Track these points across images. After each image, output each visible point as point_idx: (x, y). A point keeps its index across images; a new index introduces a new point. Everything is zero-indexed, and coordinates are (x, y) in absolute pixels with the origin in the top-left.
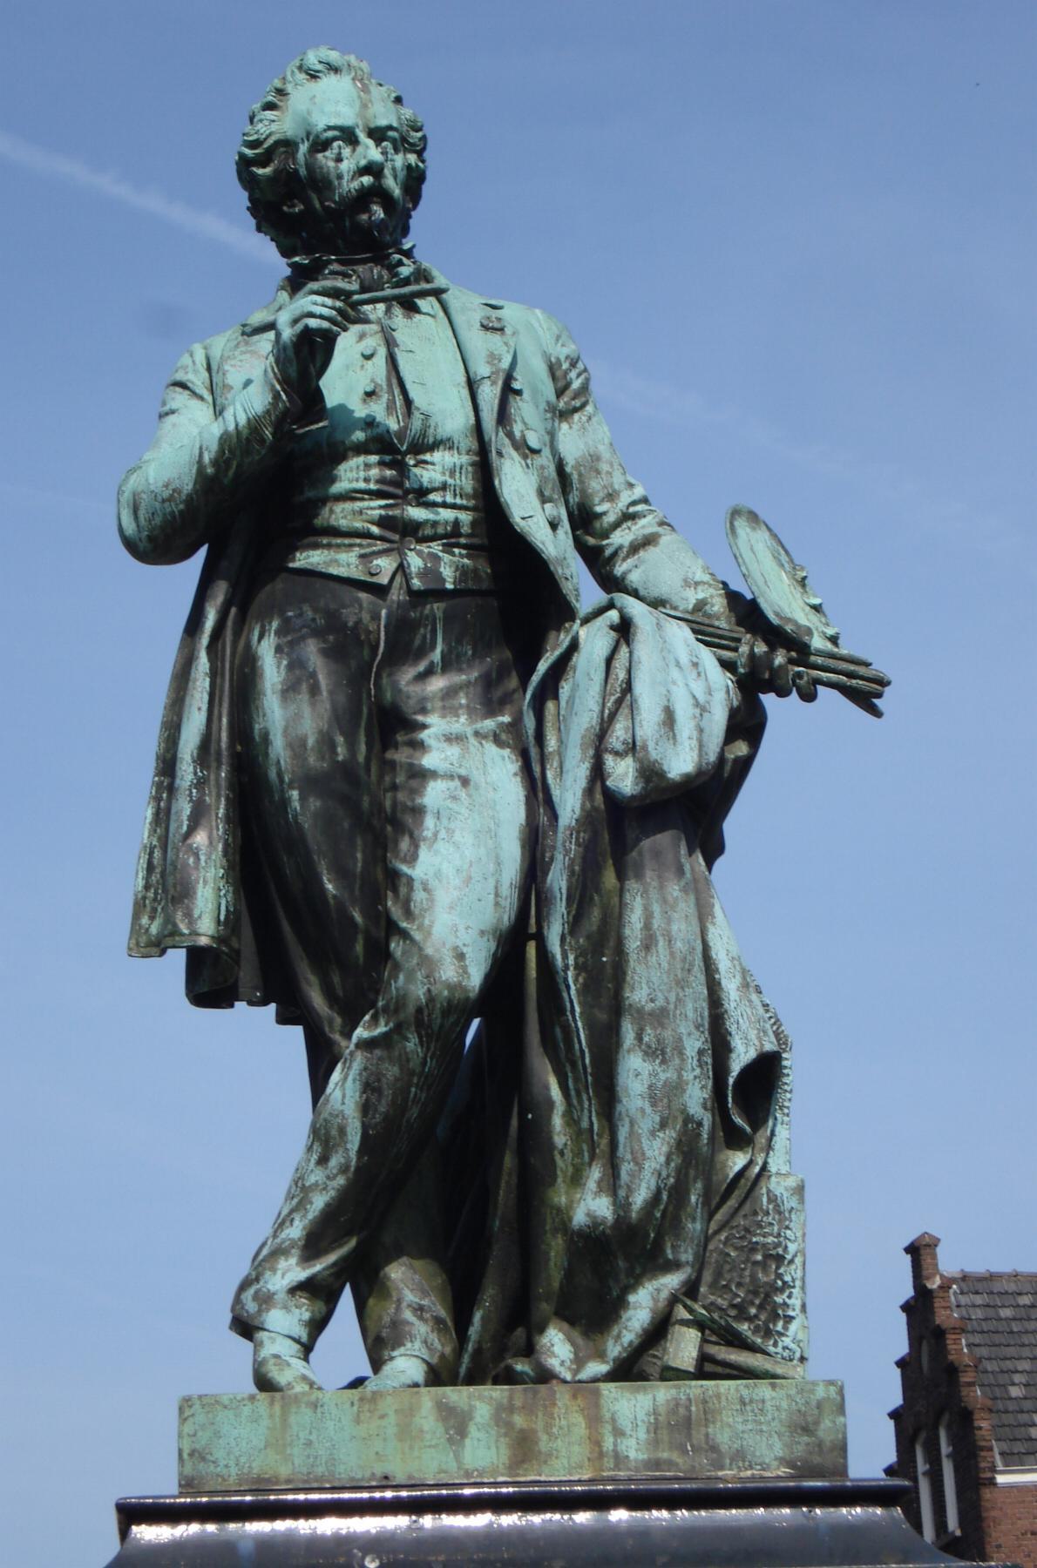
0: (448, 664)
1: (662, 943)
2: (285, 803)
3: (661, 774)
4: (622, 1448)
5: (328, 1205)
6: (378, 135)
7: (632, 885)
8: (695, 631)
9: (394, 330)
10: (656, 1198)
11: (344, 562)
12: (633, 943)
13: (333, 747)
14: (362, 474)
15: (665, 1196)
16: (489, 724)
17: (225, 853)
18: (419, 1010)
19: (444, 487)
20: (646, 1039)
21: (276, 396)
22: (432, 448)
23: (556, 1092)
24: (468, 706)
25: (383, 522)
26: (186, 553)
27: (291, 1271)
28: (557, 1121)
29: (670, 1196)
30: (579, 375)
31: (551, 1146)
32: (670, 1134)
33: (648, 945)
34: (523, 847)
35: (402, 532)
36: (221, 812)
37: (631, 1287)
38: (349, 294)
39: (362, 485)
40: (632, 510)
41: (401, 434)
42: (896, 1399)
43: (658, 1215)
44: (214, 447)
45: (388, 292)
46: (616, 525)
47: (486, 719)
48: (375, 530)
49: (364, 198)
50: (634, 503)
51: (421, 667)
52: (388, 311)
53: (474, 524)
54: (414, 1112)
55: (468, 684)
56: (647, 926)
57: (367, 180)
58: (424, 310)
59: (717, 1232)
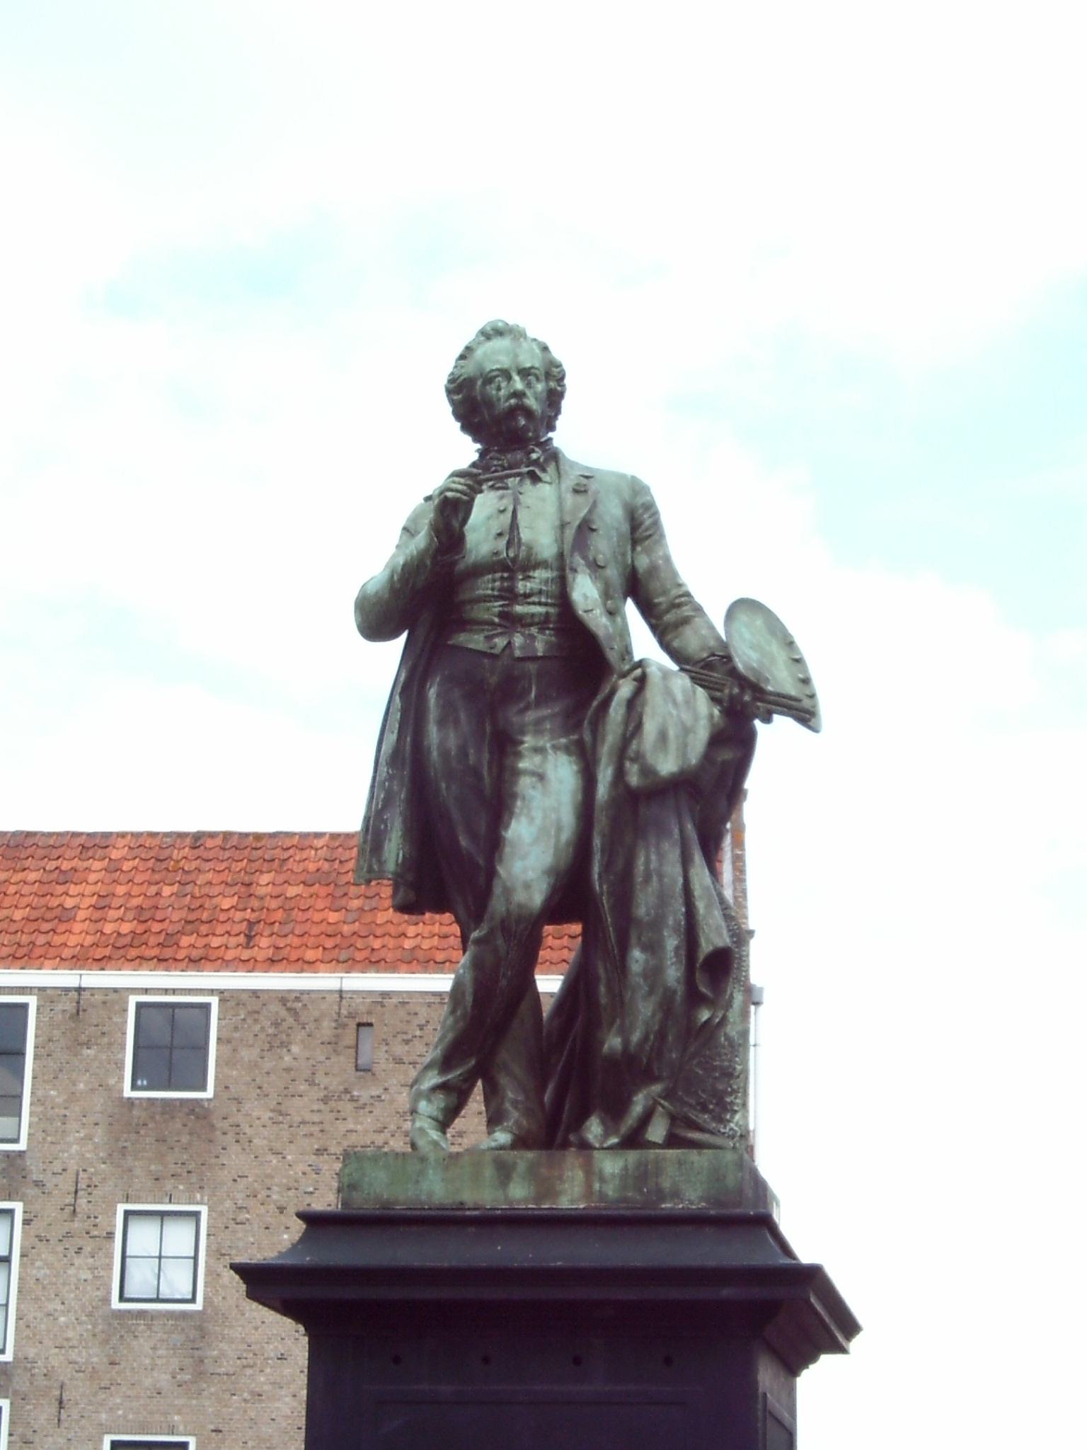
0: (539, 702)
1: (655, 878)
6: (525, 373)
8: (692, 678)
9: (521, 493)
10: (645, 1038)
11: (475, 641)
13: (466, 755)
14: (490, 586)
15: (652, 1037)
16: (563, 741)
17: (404, 822)
18: (503, 921)
19: (540, 592)
20: (643, 939)
21: (432, 540)
24: (551, 729)
25: (502, 615)
26: (393, 634)
27: (433, 1079)
28: (602, 989)
29: (655, 1037)
30: (650, 517)
32: (654, 999)
33: (647, 878)
35: (511, 621)
36: (402, 796)
37: (636, 1093)
40: (677, 601)
43: (648, 1048)
44: (399, 569)
47: (562, 737)
48: (496, 620)
49: (512, 412)
50: (676, 598)
51: (522, 705)
54: (503, 983)
57: (513, 401)
58: (544, 479)
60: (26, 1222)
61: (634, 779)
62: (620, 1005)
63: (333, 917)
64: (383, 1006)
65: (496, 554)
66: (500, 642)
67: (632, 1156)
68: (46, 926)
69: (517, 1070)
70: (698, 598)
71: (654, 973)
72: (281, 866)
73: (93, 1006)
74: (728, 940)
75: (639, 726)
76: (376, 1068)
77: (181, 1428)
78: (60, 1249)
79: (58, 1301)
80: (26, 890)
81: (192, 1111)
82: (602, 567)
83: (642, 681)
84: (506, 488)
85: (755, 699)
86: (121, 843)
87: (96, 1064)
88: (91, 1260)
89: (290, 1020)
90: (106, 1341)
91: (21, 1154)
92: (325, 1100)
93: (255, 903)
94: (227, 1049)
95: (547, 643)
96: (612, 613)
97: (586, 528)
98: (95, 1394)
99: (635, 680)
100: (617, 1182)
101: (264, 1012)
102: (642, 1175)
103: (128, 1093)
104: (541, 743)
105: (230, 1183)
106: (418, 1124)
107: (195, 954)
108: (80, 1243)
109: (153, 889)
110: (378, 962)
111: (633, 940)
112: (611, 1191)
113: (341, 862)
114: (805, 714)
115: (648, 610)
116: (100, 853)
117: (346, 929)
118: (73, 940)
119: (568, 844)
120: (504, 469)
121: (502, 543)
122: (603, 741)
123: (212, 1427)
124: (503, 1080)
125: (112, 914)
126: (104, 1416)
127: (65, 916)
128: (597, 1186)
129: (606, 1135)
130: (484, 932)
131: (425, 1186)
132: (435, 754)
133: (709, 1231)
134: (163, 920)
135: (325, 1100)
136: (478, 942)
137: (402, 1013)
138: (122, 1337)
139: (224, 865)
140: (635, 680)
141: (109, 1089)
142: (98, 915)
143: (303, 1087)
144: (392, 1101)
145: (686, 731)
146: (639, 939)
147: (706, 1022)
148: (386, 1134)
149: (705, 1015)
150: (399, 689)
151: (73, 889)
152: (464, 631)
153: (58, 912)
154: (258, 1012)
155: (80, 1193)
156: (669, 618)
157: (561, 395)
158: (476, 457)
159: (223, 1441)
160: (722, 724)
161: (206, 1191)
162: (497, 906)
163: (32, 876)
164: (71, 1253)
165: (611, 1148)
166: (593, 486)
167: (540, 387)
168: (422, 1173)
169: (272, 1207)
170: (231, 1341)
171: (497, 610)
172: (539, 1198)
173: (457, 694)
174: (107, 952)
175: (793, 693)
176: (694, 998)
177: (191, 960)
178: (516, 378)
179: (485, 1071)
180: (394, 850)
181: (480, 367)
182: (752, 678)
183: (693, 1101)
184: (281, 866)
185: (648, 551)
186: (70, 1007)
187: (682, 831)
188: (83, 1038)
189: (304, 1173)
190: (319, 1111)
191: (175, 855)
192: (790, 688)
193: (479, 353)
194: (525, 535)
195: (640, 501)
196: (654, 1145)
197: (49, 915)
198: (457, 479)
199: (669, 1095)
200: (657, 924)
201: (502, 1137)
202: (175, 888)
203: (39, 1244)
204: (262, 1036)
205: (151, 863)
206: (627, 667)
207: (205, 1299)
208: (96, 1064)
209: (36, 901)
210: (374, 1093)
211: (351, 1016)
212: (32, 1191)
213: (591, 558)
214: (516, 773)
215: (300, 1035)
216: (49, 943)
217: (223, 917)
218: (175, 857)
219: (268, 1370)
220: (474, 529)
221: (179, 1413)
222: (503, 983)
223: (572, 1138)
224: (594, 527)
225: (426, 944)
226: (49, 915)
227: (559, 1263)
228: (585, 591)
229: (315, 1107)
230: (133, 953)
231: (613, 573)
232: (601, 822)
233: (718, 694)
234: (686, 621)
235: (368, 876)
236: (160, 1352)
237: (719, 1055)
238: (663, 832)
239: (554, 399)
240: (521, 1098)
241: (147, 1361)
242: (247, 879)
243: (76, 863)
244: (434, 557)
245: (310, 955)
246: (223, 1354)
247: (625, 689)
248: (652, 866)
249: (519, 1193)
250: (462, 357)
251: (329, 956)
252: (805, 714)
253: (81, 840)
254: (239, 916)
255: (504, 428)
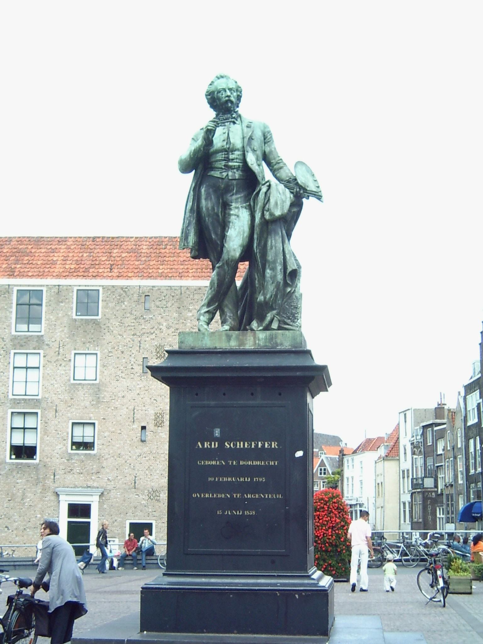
0: (236, 194)
2: (205, 221)
3: (274, 215)
4: (260, 343)
5: (211, 297)
6: (230, 90)
7: (269, 237)
8: (285, 186)
10: (271, 296)
11: (217, 174)
12: (269, 248)
13: (214, 210)
15: (273, 296)
16: (244, 205)
17: (195, 230)
19: (237, 158)
22: (235, 151)
23: (256, 277)
25: (225, 166)
27: (205, 309)
28: (257, 282)
31: (255, 286)
32: (274, 285)
33: (271, 248)
34: (249, 229)
35: (228, 168)
36: (194, 222)
38: (217, 122)
39: (221, 158)
40: (278, 162)
41: (229, 148)
42: (480, 341)
44: (193, 151)
45: (230, 120)
46: (275, 165)
48: (223, 167)
49: (227, 102)
50: (279, 160)
52: (230, 124)
53: (243, 165)
54: (227, 280)
55: (241, 197)
56: (271, 245)
57: (227, 98)
59: (285, 303)
60: (44, 356)
61: (267, 216)
62: (263, 287)
63: (137, 263)
64: (153, 290)
65: (223, 146)
66: (225, 174)
67: (268, 332)
68: (48, 266)
69: (230, 307)
70: (285, 161)
71: (274, 277)
72: (120, 247)
73: (63, 290)
74: (296, 267)
75: (269, 200)
76: (151, 309)
77: (93, 418)
78: (55, 364)
79: (54, 380)
80: (41, 255)
81: (94, 323)
82: (255, 151)
83: (269, 186)
84: (225, 126)
85: (304, 192)
86: (70, 240)
87: (64, 308)
88: (64, 368)
89: (124, 294)
90: (69, 392)
91: (42, 336)
92: (135, 319)
93: (113, 259)
94: (105, 303)
95: (239, 174)
96: (259, 165)
97: (251, 138)
98: (67, 408)
99: (267, 186)
100: (263, 340)
101: (116, 292)
102: (271, 338)
103: (75, 317)
104: (237, 206)
105: (106, 344)
106: (200, 323)
107: (94, 274)
108: (61, 363)
109: (81, 254)
110: (151, 277)
111: (267, 266)
112: (262, 343)
113: (139, 246)
114: (319, 197)
115: (269, 164)
116: (64, 243)
117: (141, 267)
118: (56, 270)
119: (246, 237)
120: (224, 120)
121: (225, 143)
122: (257, 205)
123: (102, 418)
124: (226, 310)
125: (68, 262)
126: (69, 415)
127: (54, 263)
128: (257, 342)
129: (258, 327)
130: (221, 264)
131: (204, 342)
132: (204, 209)
133: (292, 355)
134: (84, 264)
135: (135, 319)
136: (219, 267)
137: (158, 292)
138: (74, 391)
139: (103, 247)
140: (267, 186)
141: (69, 316)
142: (64, 262)
143: (128, 315)
144: (156, 319)
145: (283, 202)
146: (269, 266)
147: (289, 292)
148: (154, 329)
149: (289, 289)
150: (192, 189)
151: (56, 255)
152: (213, 171)
153: (52, 261)
154: (114, 292)
155: (60, 348)
156: (275, 167)
157: (241, 97)
158: (215, 116)
159: (106, 422)
160: (293, 200)
161: (99, 347)
162: (225, 256)
163: (43, 251)
164: (58, 365)
165: (260, 330)
166: (252, 125)
167: (235, 94)
168: (203, 338)
169: (119, 352)
170: (108, 392)
171: (223, 164)
172: (239, 346)
173: (211, 190)
174: (67, 274)
175: (315, 190)
176: (286, 285)
177: (93, 276)
178: (228, 91)
179: (220, 308)
180: (192, 239)
181: (217, 89)
182: (303, 186)
183: (285, 316)
184: (120, 247)
185: (269, 146)
186: (56, 291)
187: (282, 234)
188: (61, 300)
189: (129, 341)
190: (133, 322)
191: (87, 243)
192: (314, 189)
193: (215, 84)
194: (232, 141)
195: (266, 130)
196: (274, 329)
197: (49, 263)
198: (211, 123)
199: (278, 314)
200: (275, 262)
201: (227, 327)
202: (88, 254)
203: (48, 363)
204: (116, 299)
205: (80, 246)
206: (263, 182)
207: (100, 379)
208: (64, 308)
209: (44, 258)
210: (151, 317)
211: (143, 293)
212: (46, 347)
213: (252, 148)
214: (230, 215)
215: (127, 299)
216: (49, 271)
217: (103, 263)
218: (87, 244)
219: (119, 401)
220: (215, 139)
221: (92, 414)
222: (227, 280)
223: (248, 327)
224: (253, 138)
225: (166, 271)
226: (49, 263)
227: (247, 365)
228: (251, 159)
229: (132, 321)
230: (75, 274)
231: (259, 153)
232: (257, 230)
233: (292, 191)
234: (281, 168)
235: (183, 247)
236: (86, 395)
237: (293, 301)
238: (276, 233)
239: (239, 98)
240: (232, 315)
241: (82, 398)
242: (110, 251)
243: (57, 246)
244: (204, 148)
245: (130, 275)
246: (105, 396)
247: (264, 189)
248: (273, 244)
249: (233, 345)
250: (211, 85)
251: (136, 275)
252: (319, 197)
253: (58, 239)
254: (107, 263)
255: (224, 107)
